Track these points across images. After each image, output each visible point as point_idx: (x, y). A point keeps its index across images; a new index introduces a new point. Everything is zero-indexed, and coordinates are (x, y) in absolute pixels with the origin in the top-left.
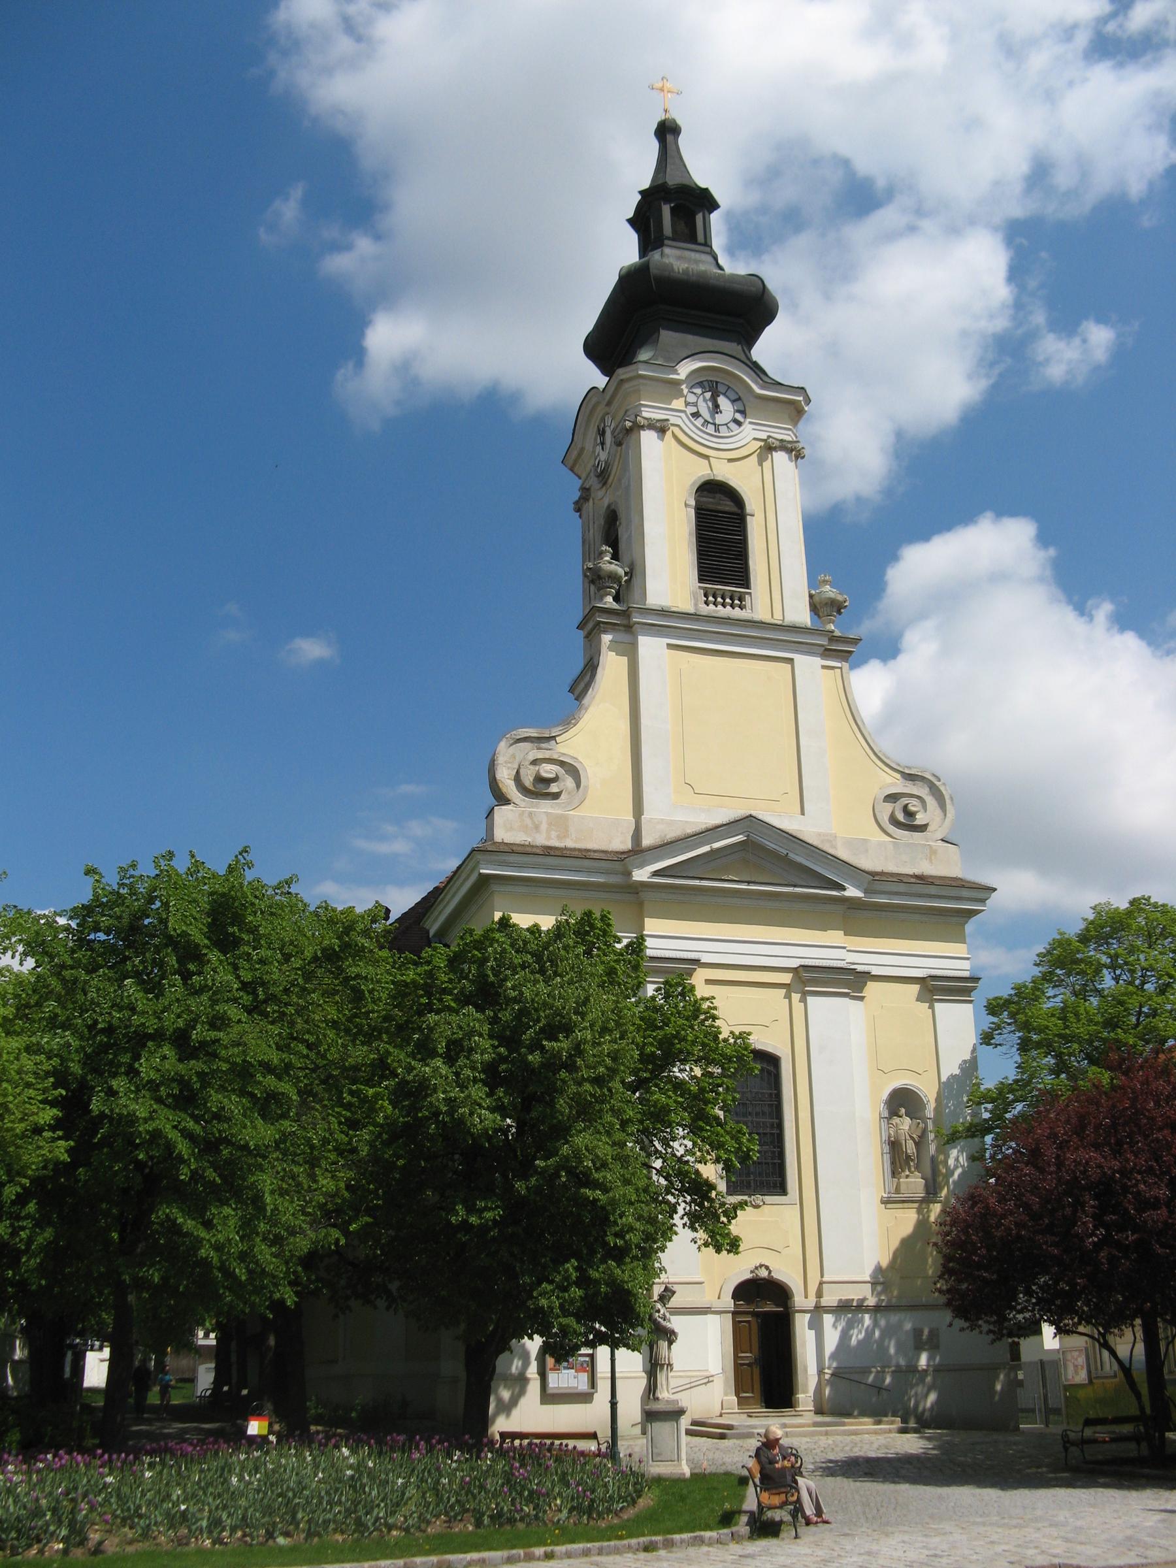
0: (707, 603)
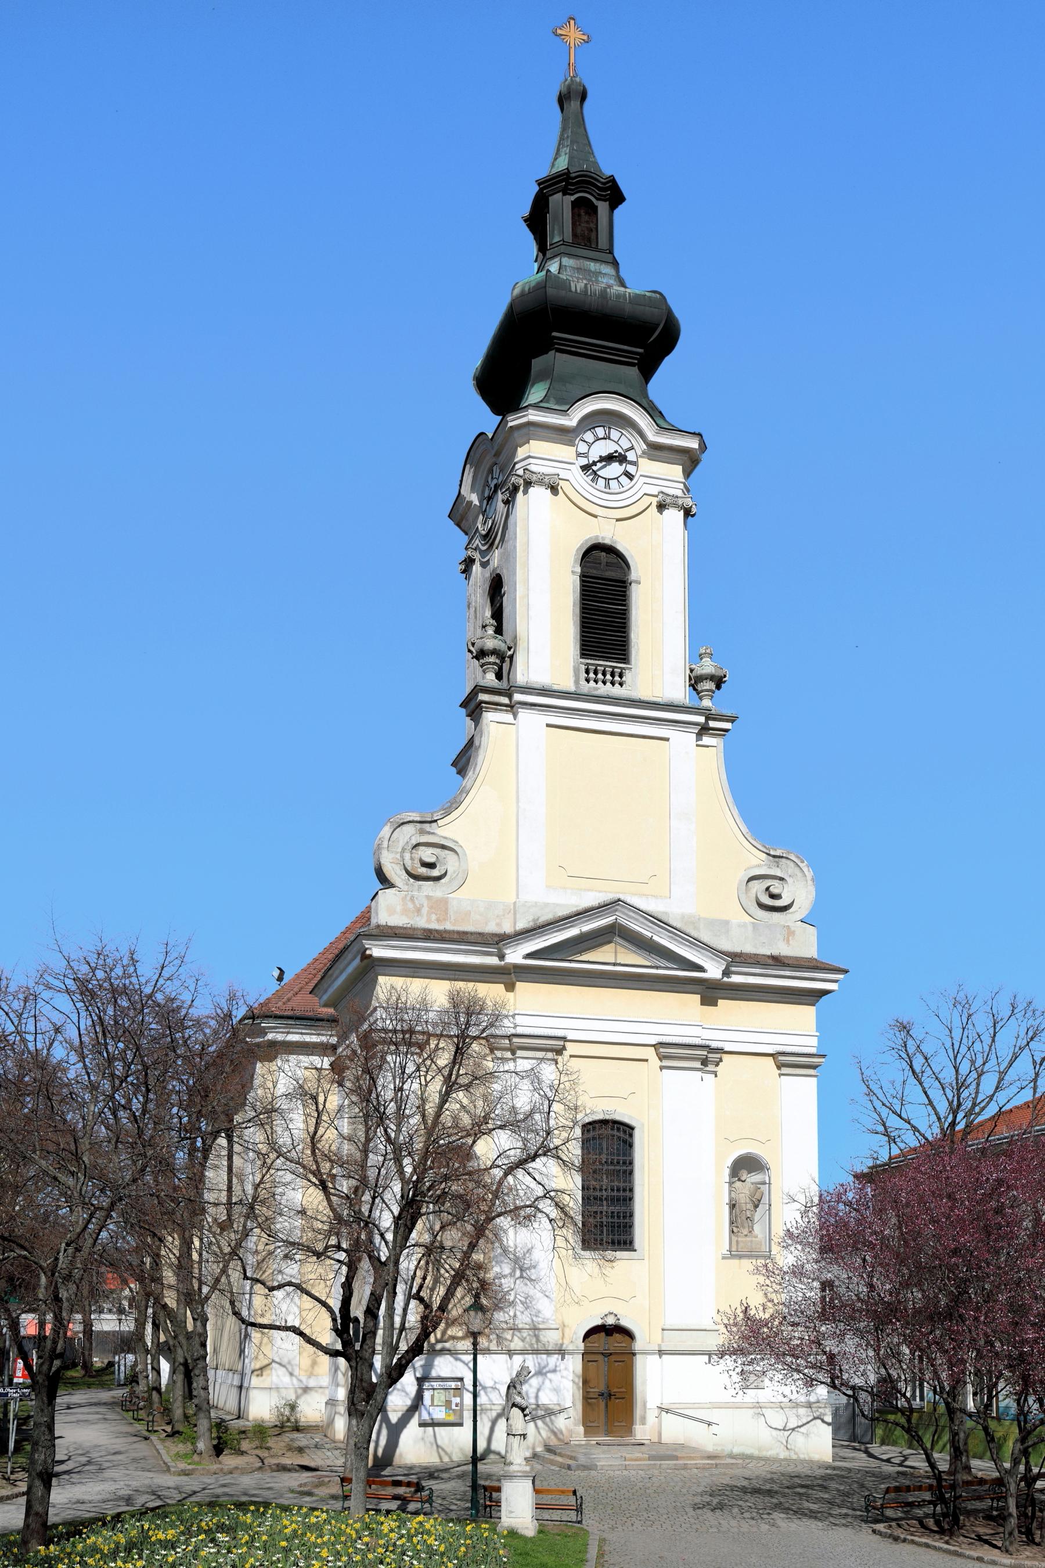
0: (588, 680)
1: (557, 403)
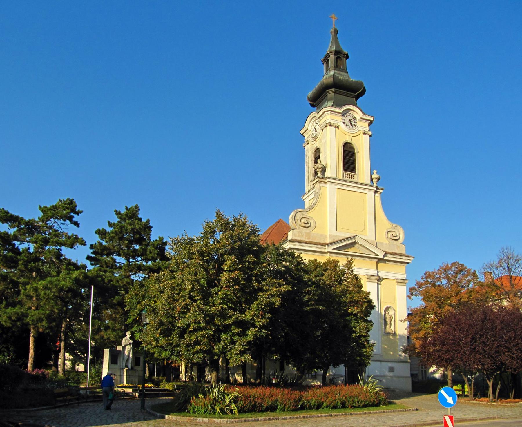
1: (91, 360)
